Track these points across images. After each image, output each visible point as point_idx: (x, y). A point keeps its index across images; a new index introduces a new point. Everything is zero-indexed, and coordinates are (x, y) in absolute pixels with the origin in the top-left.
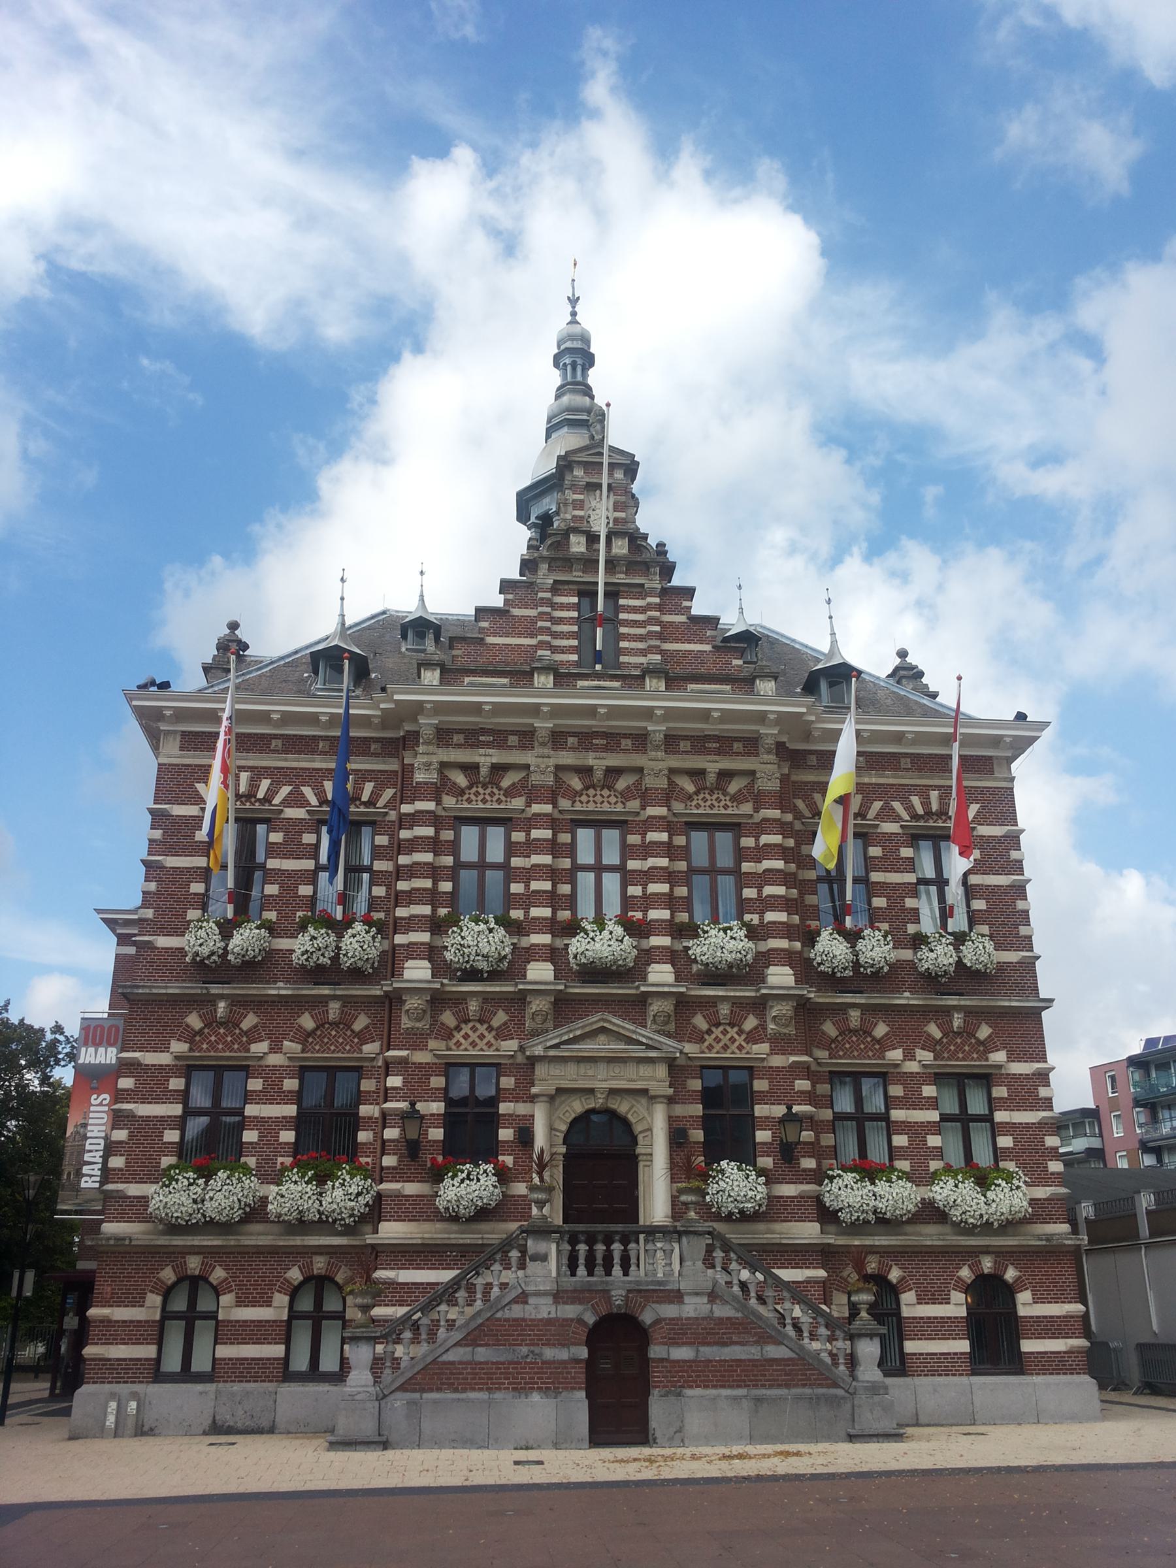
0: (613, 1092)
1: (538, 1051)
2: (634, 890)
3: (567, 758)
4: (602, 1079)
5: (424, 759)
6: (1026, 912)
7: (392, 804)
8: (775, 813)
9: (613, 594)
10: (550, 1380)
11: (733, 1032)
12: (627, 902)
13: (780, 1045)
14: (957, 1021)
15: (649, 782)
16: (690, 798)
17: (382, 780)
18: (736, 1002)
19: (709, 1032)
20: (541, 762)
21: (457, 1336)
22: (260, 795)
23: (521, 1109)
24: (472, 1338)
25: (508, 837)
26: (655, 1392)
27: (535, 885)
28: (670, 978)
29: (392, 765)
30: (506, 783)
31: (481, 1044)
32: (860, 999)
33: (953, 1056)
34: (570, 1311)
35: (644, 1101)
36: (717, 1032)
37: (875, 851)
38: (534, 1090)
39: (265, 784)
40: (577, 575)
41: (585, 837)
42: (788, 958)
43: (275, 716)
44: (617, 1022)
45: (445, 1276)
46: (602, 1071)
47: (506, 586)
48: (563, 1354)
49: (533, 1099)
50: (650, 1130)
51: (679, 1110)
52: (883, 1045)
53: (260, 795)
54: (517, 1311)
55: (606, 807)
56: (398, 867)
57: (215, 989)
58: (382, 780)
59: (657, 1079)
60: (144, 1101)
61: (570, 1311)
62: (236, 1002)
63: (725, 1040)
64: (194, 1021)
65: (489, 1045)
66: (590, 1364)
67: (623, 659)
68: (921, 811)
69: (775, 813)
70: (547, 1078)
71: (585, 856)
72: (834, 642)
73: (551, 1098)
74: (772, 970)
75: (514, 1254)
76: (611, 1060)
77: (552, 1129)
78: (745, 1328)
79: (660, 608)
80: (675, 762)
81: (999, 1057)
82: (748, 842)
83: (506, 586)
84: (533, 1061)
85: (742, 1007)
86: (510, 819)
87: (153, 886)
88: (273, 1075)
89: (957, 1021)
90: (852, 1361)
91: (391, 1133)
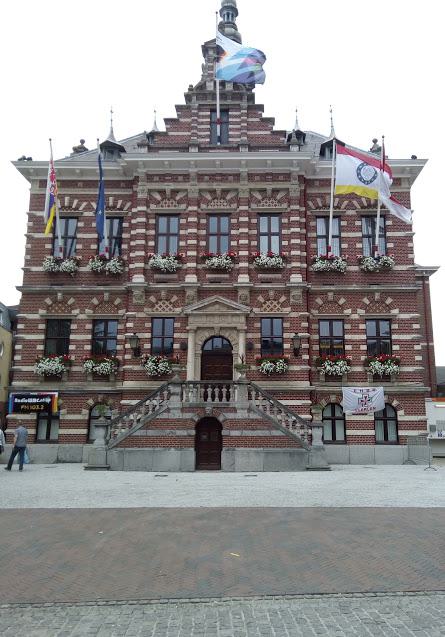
0: (221, 328)
1: (189, 311)
2: (285, 243)
3: (204, 186)
4: (217, 323)
5: (141, 188)
6: (27, 253)
7: (130, 208)
8: (297, 207)
9: (225, 111)
10: (179, 444)
11: (275, 303)
12: (281, 248)
13: (295, 308)
14: (377, 296)
15: (241, 195)
16: (260, 202)
17: (126, 198)
18: (276, 290)
19: (265, 303)
20: (244, 186)
21: (140, 425)
22: (74, 207)
23: (183, 336)
24: (146, 426)
25: (280, 221)
26: (224, 449)
27: (189, 242)
28: (248, 280)
29: (128, 192)
30: (178, 198)
31: (167, 309)
32: (332, 288)
33: (375, 312)
34: (188, 416)
35: (235, 332)
36: (268, 303)
37: (343, 223)
38: (188, 328)
39: (76, 202)
40: (209, 102)
41: (264, 220)
42: (299, 270)
43: (78, 171)
44: (227, 301)
45: (134, 402)
46: (217, 319)
47: (178, 108)
48: (184, 433)
49: (188, 331)
50: (237, 344)
51: (250, 336)
52: (342, 307)
53: (74, 207)
54: (165, 416)
55: (222, 207)
56: (132, 235)
57: (56, 288)
58: (126, 198)
59: (241, 323)
60: (28, 333)
61: (188, 416)
62: (65, 293)
63: (272, 306)
64: (48, 301)
65: (170, 310)
66: (197, 438)
67: (230, 140)
68: (366, 204)
69: (297, 207)
70: (193, 324)
71: (264, 229)
72: (332, 130)
73: (196, 331)
74: (293, 276)
75: (165, 393)
76: (220, 315)
77: (196, 344)
78: (266, 423)
79: (248, 115)
80: (252, 186)
81: (395, 311)
82: (285, 220)
83: (178, 108)
84: (187, 316)
85: (279, 292)
86: (179, 214)
87: (29, 246)
88: (81, 323)
89: (377, 296)
90: (311, 437)
91: (128, 346)
